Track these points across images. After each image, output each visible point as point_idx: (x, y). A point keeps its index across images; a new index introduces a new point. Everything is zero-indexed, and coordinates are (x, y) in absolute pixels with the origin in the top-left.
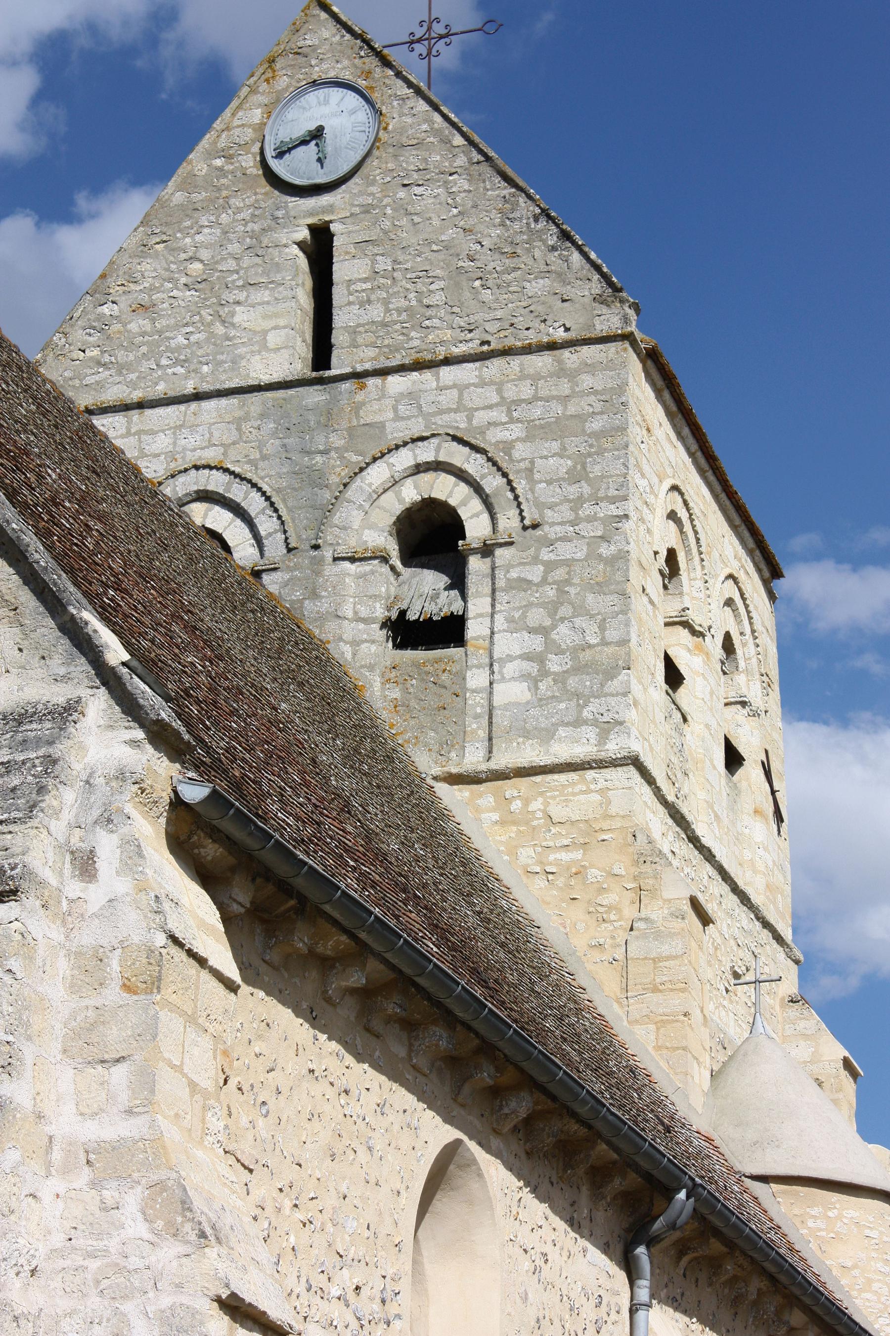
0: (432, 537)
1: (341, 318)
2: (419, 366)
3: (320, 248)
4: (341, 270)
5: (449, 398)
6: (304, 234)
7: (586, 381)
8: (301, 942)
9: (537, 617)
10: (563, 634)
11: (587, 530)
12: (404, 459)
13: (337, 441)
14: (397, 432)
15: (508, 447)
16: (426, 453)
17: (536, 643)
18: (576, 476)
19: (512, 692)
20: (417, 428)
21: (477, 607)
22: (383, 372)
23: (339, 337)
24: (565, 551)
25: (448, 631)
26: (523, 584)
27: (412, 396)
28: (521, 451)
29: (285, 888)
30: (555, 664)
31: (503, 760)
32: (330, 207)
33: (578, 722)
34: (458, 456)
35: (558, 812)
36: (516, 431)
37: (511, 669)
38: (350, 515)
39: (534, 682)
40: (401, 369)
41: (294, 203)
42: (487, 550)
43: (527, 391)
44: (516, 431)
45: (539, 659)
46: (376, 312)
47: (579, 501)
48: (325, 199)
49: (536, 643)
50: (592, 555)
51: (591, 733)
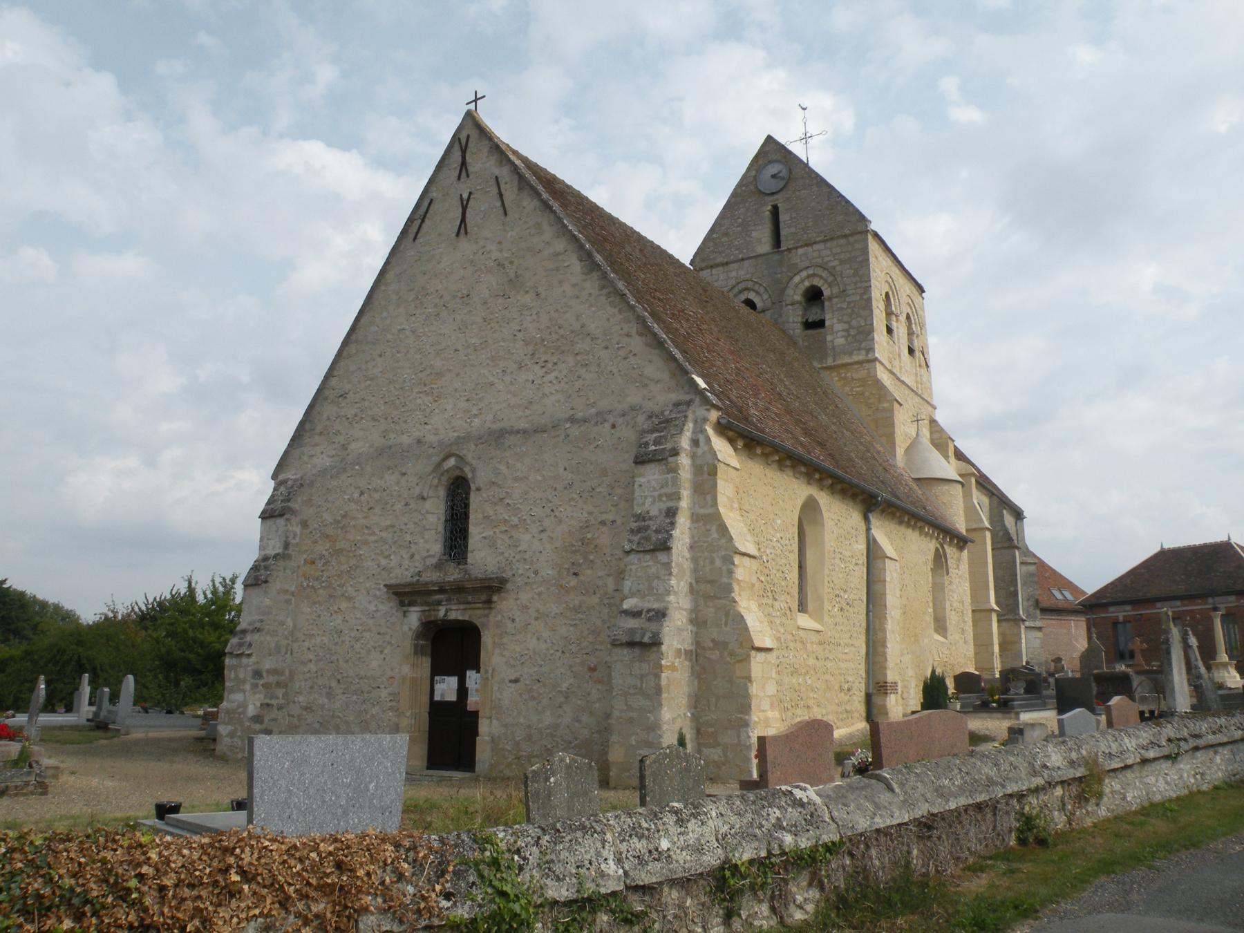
0: (814, 296)
1: (783, 232)
2: (807, 245)
3: (775, 212)
4: (782, 218)
5: (816, 254)
6: (769, 208)
7: (856, 246)
8: (759, 451)
9: (846, 318)
10: (854, 323)
11: (859, 291)
12: (804, 274)
13: (784, 269)
14: (802, 265)
15: (834, 267)
16: (811, 271)
17: (846, 326)
18: (855, 275)
19: (840, 341)
20: (808, 264)
21: (828, 316)
22: (796, 248)
23: (782, 238)
24: (853, 298)
25: (820, 324)
26: (841, 309)
27: (804, 254)
28: (838, 268)
29: (753, 440)
30: (852, 332)
31: (839, 362)
32: (779, 200)
33: (859, 349)
34: (819, 271)
35: (855, 376)
36: (836, 263)
37: (840, 334)
38: (790, 292)
39: (846, 338)
40: (802, 247)
41: (767, 198)
42: (830, 299)
43: (839, 250)
44: (836, 263)
45: (847, 330)
46: (793, 230)
47: (856, 283)
48: (776, 197)
49: (846, 326)
50: (861, 298)
51: (863, 352)
